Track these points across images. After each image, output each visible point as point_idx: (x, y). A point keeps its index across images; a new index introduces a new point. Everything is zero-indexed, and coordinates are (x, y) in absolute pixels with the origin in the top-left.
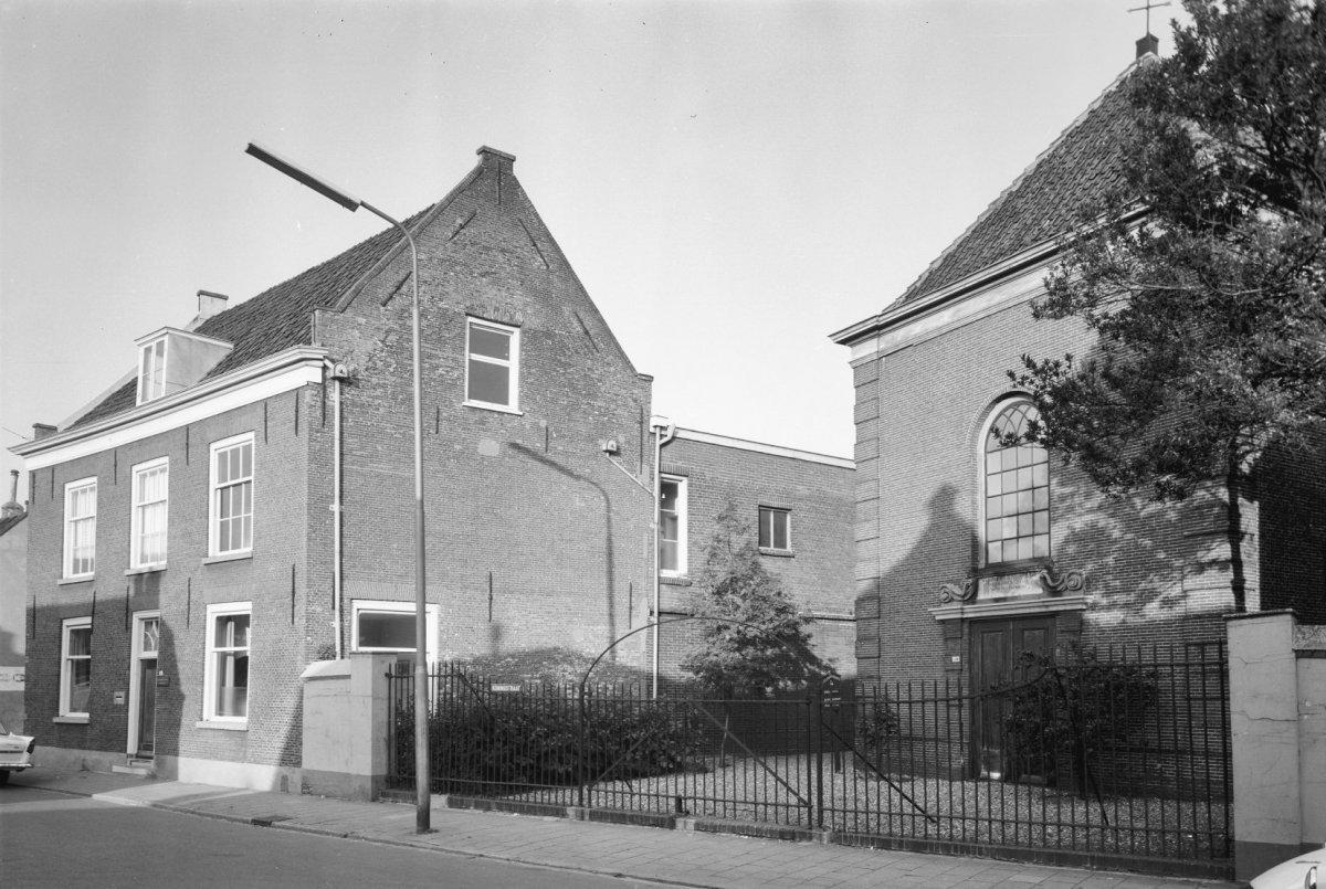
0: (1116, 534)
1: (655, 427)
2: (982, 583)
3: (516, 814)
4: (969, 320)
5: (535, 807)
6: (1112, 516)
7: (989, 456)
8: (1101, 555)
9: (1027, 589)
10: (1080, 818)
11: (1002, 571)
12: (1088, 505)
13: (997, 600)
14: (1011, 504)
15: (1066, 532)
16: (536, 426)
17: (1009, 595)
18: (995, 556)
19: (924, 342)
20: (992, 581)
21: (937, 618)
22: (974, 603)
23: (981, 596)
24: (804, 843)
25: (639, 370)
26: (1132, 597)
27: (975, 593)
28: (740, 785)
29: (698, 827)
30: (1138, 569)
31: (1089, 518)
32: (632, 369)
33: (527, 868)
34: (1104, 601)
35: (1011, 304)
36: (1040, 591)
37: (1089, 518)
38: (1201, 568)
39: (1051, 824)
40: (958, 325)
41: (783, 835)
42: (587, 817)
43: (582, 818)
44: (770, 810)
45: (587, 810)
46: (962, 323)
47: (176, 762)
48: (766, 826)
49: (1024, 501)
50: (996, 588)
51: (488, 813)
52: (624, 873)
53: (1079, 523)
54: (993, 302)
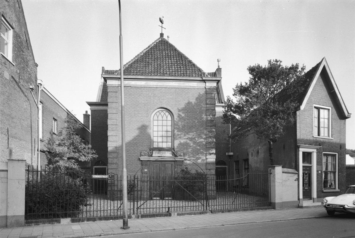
0: (192, 145)
1: (39, 84)
2: (154, 152)
3: (111, 220)
4: (150, 86)
5: (118, 217)
6: (190, 141)
7: (154, 121)
8: (187, 149)
9: (168, 155)
10: (195, 205)
11: (160, 149)
12: (184, 138)
13: (159, 156)
14: (160, 134)
15: (179, 143)
16: (16, 72)
17: (162, 155)
18: (155, 145)
19: (136, 87)
20: (157, 152)
21: (141, 160)
22: (152, 156)
23: (153, 155)
24: (206, 214)
25: (36, 62)
26: (194, 159)
27: (152, 154)
28: (102, 205)
29: (178, 215)
30: (196, 152)
31: (185, 140)
32: (34, 61)
33: (203, 228)
34: (188, 159)
35: (164, 87)
36: (171, 155)
37: (185, 140)
38: (211, 154)
39: (99, 211)
40: (146, 86)
41: (200, 213)
42: (140, 217)
43: (138, 218)
44: (176, 208)
45: (140, 215)
46: (148, 86)
47: (277, 203)
48: (196, 212)
49: (164, 134)
50: (158, 153)
51: (96, 222)
52: (224, 224)
53: (182, 141)
54: (158, 85)
